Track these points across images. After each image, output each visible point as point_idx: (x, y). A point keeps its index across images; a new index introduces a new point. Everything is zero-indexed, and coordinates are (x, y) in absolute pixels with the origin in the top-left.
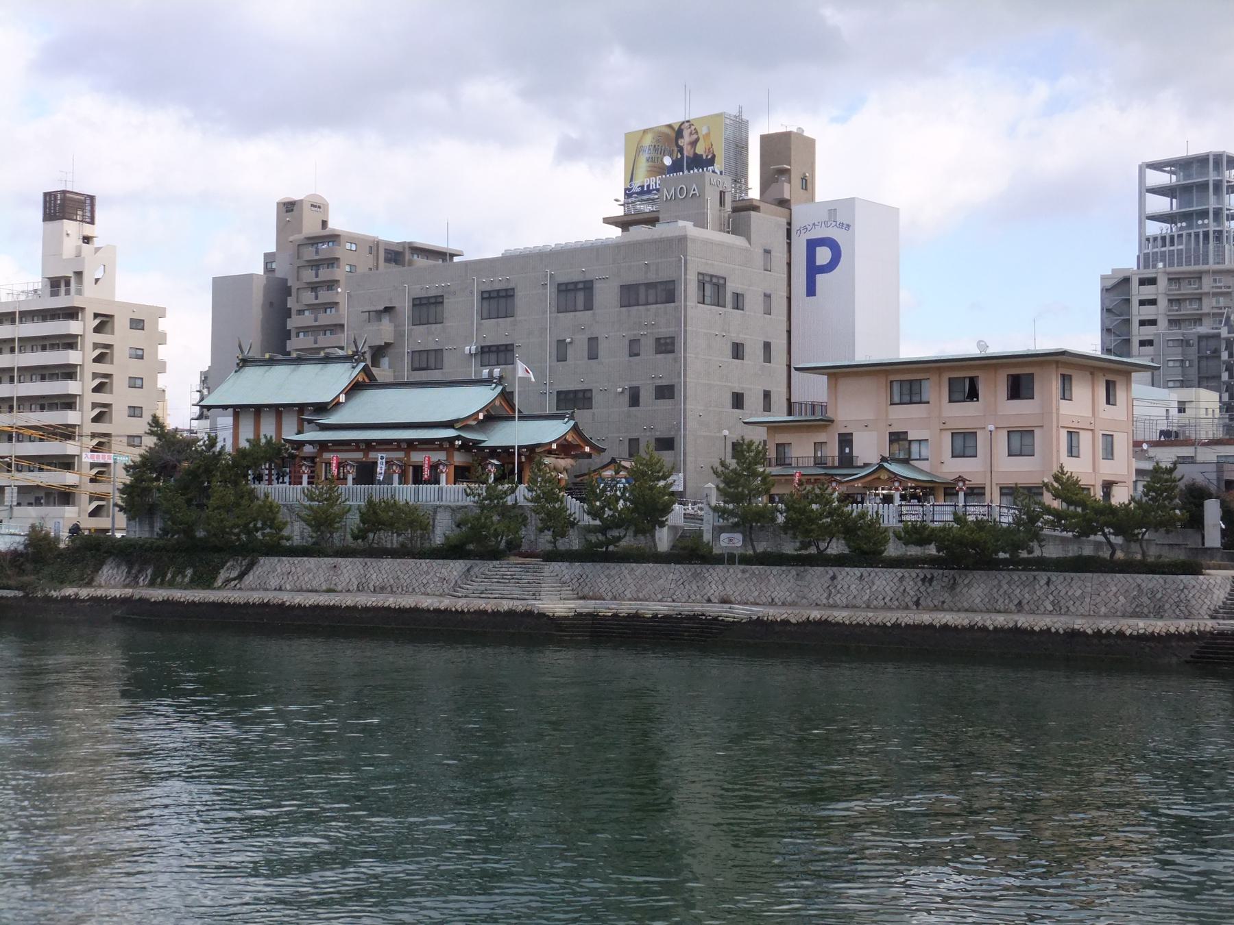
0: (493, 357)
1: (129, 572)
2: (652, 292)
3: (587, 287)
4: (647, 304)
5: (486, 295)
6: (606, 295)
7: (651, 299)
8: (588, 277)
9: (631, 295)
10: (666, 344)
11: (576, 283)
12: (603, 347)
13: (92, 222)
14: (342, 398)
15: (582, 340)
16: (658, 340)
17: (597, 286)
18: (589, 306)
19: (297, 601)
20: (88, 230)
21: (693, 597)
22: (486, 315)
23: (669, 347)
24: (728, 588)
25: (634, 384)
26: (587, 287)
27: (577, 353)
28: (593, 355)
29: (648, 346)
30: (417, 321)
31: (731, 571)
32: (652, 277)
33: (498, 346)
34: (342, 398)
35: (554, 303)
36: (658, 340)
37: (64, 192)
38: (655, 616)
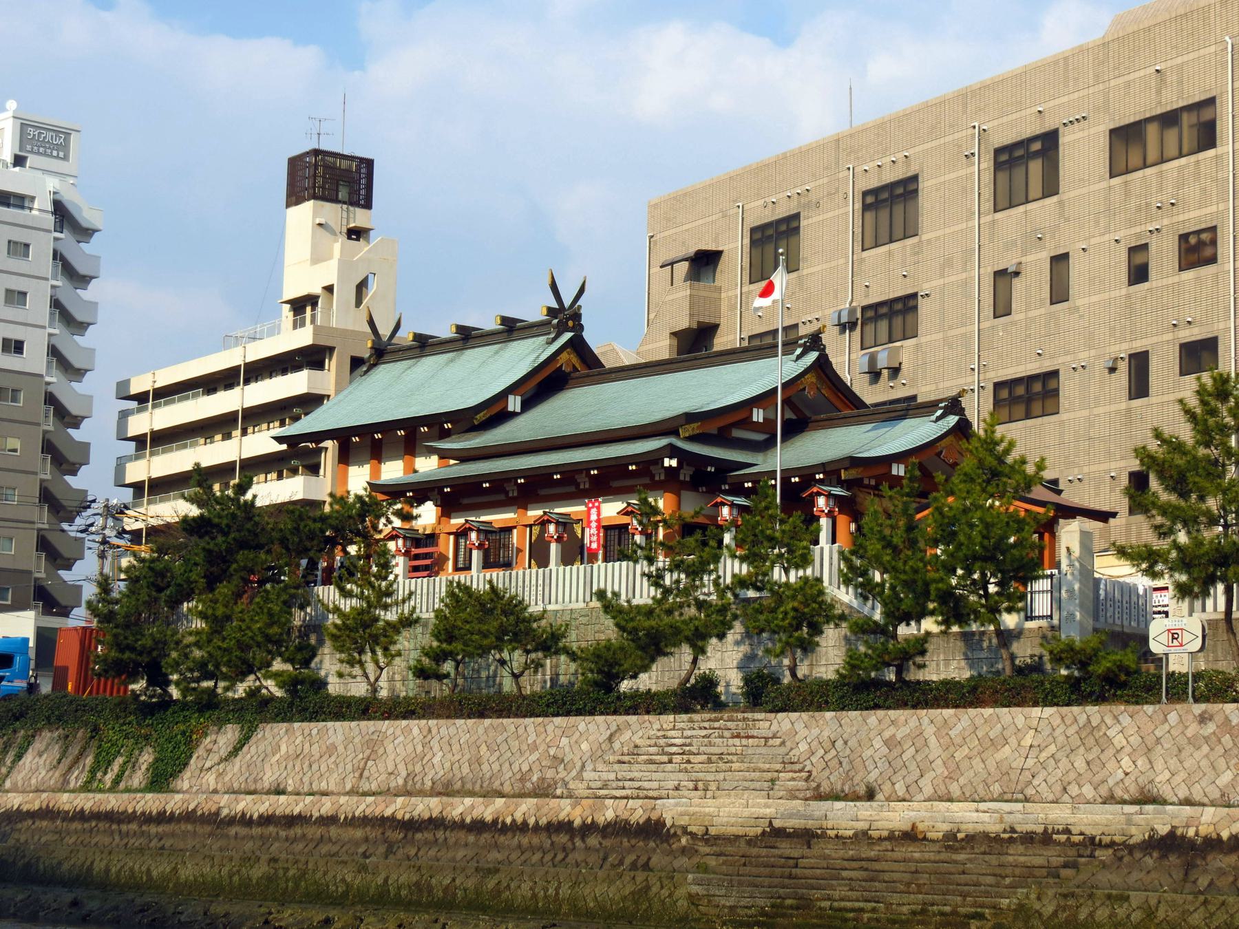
0: (883, 325)
1: (64, 754)
2: (1171, 135)
3: (1048, 144)
4: (1163, 160)
5: (870, 200)
6: (1083, 153)
7: (1172, 149)
8: (1048, 126)
9: (1129, 143)
10: (1201, 244)
11: (1024, 143)
12: (1077, 269)
13: (368, 205)
14: (514, 403)
15: (1037, 265)
16: (1184, 238)
17: (1065, 139)
18: (1051, 188)
19: (240, 807)
20: (360, 218)
21: (1074, 790)
22: (873, 239)
23: (1208, 252)
24: (1159, 765)
25: (1138, 346)
26: (1048, 144)
27: (1031, 289)
28: (1059, 293)
29: (1163, 255)
30: (760, 272)
31: (1173, 717)
32: (1172, 100)
33: (890, 303)
34: (514, 403)
35: (988, 192)
36: (1184, 238)
37: (316, 152)
38: (950, 836)
